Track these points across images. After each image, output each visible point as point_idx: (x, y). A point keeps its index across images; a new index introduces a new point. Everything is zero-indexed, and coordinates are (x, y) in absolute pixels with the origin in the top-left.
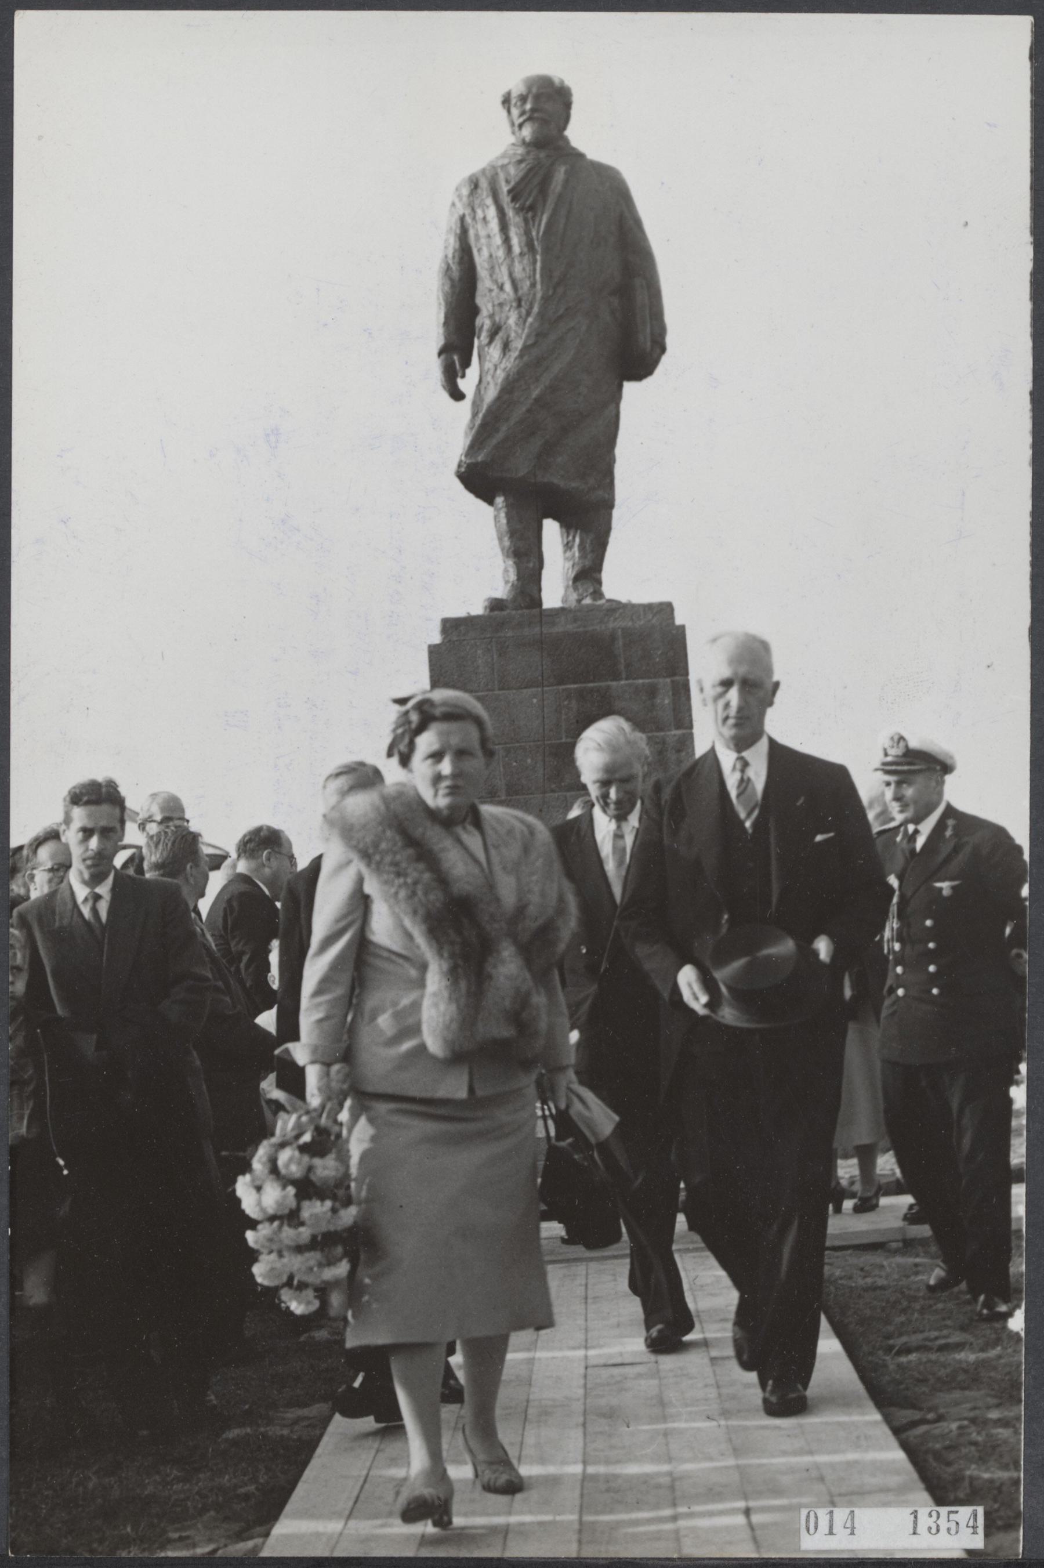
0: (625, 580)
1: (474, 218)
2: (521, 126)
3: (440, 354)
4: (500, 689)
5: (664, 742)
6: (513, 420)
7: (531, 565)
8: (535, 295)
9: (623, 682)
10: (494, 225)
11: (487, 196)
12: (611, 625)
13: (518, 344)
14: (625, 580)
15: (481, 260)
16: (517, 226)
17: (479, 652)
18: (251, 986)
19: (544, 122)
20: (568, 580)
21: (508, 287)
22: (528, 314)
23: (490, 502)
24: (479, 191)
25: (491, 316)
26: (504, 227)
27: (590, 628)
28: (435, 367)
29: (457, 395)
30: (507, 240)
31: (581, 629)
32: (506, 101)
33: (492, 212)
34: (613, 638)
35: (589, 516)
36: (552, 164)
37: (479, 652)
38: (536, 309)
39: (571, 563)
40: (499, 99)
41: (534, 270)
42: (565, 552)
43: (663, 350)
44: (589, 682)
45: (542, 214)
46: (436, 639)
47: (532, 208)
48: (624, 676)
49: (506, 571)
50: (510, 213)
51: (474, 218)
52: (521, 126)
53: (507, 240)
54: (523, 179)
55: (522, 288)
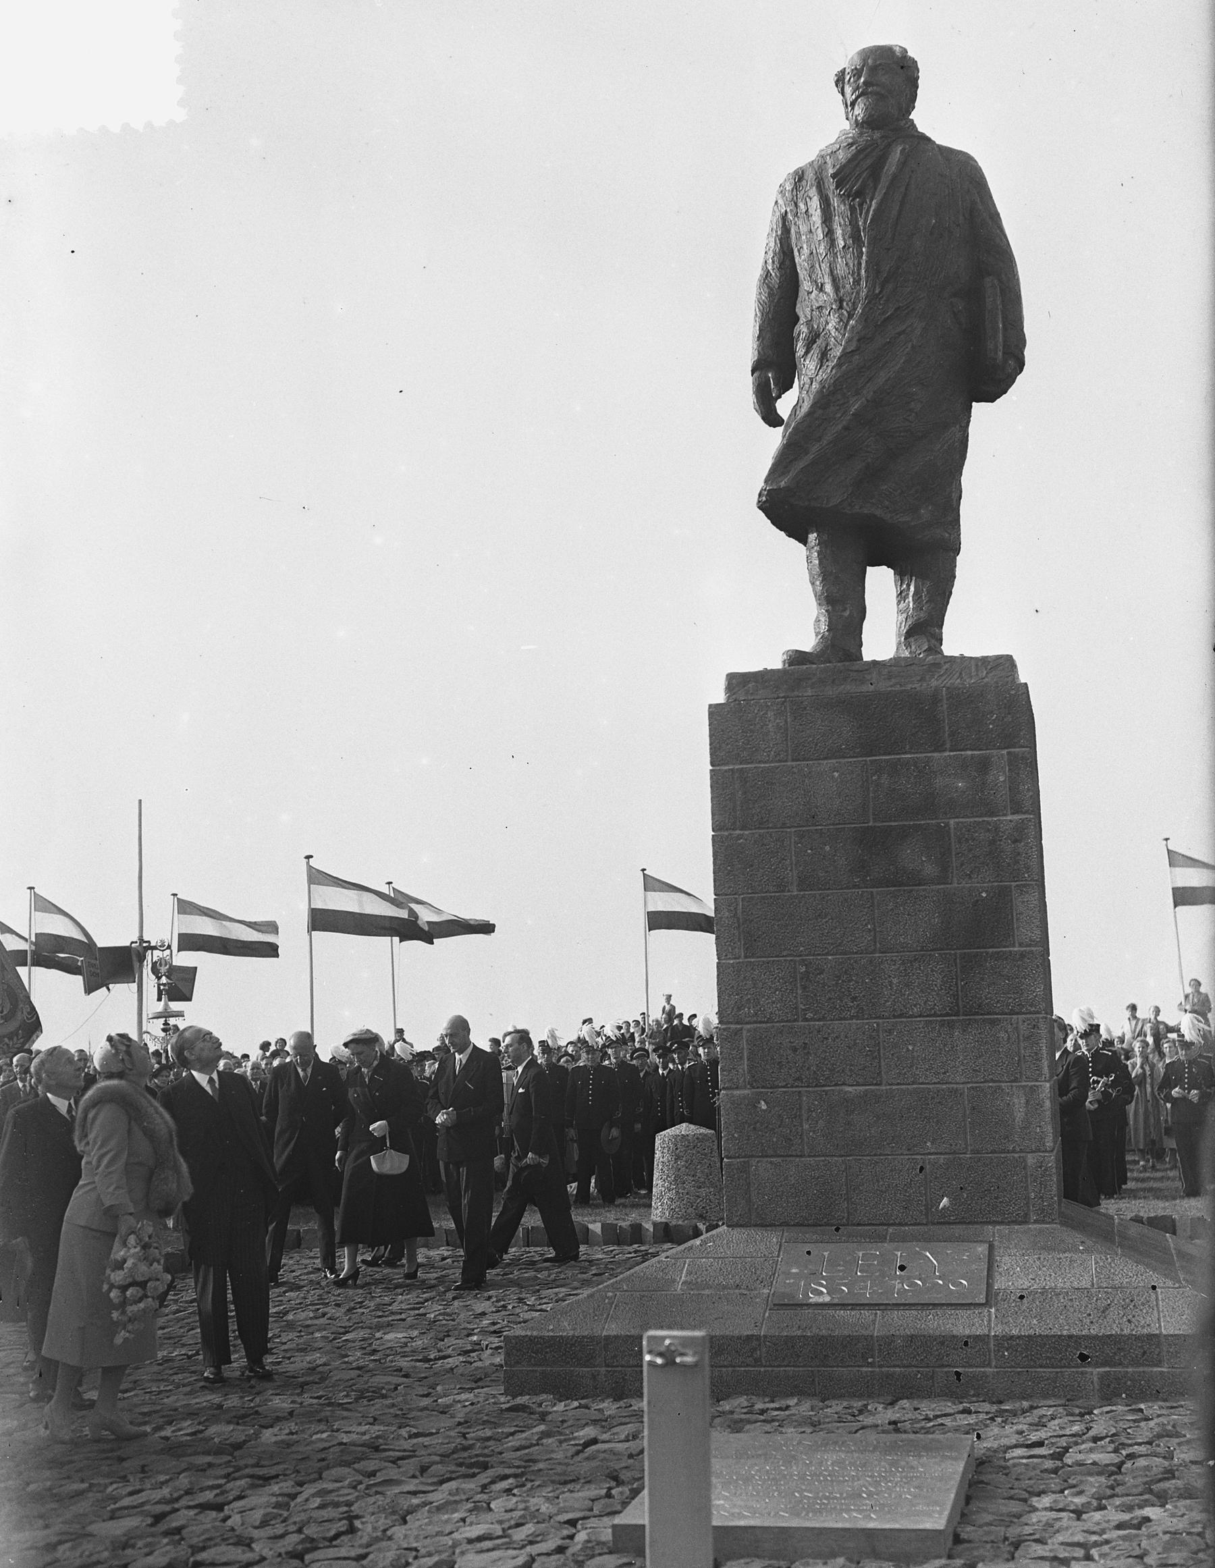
0: (964, 636)
1: (796, 215)
2: (853, 104)
3: (753, 372)
4: (793, 760)
5: (997, 829)
6: (828, 437)
7: (847, 613)
8: (858, 293)
9: (947, 754)
10: (817, 217)
11: (812, 185)
12: (934, 683)
13: (837, 352)
14: (964, 636)
15: (801, 261)
16: (842, 214)
17: (770, 714)
18: (442, 1124)
19: (880, 97)
20: (899, 635)
21: (828, 288)
22: (850, 316)
23: (803, 540)
24: (804, 183)
25: (809, 323)
26: (827, 219)
27: (909, 687)
28: (746, 385)
29: (772, 419)
30: (830, 234)
31: (898, 688)
32: (840, 80)
33: (815, 203)
34: (935, 698)
35: (929, 561)
36: (889, 145)
37: (770, 714)
38: (859, 310)
39: (905, 615)
40: (833, 79)
41: (860, 264)
42: (899, 603)
43: (1021, 365)
44: (905, 753)
45: (871, 201)
46: (720, 697)
47: (859, 194)
48: (948, 746)
49: (818, 621)
50: (835, 202)
51: (796, 215)
52: (853, 104)
53: (830, 234)
54: (850, 161)
55: (844, 287)
